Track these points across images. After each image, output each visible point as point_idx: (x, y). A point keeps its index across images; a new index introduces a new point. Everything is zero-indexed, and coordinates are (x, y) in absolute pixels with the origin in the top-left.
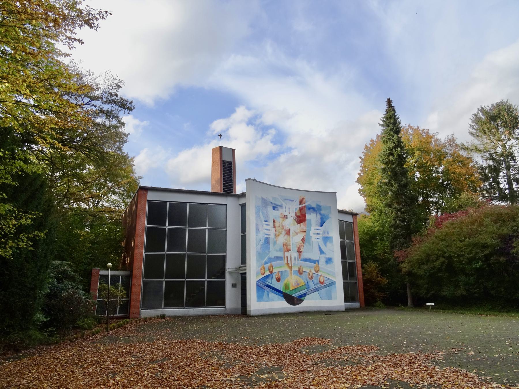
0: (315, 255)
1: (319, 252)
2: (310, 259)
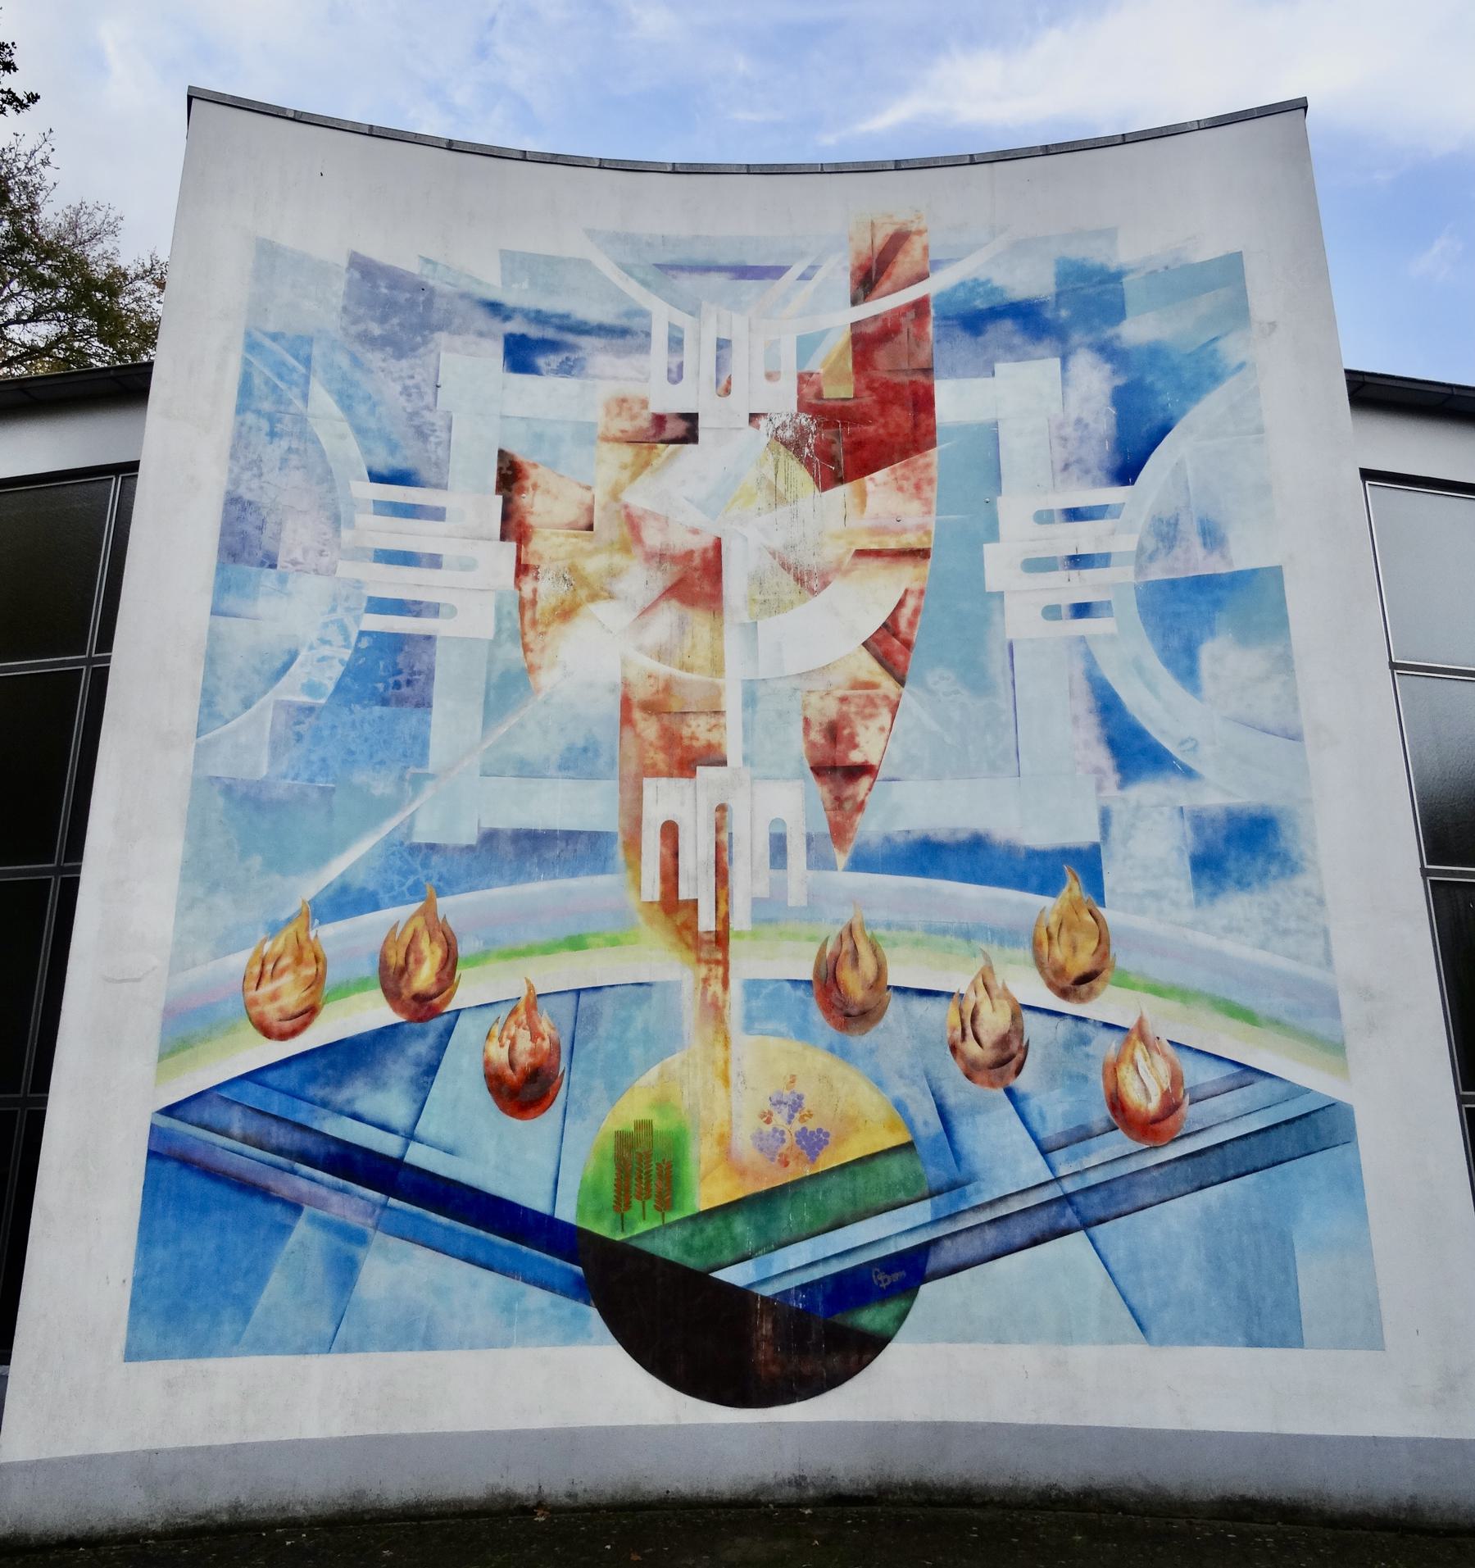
0: (1050, 796)
1: (1102, 758)
2: (977, 844)
